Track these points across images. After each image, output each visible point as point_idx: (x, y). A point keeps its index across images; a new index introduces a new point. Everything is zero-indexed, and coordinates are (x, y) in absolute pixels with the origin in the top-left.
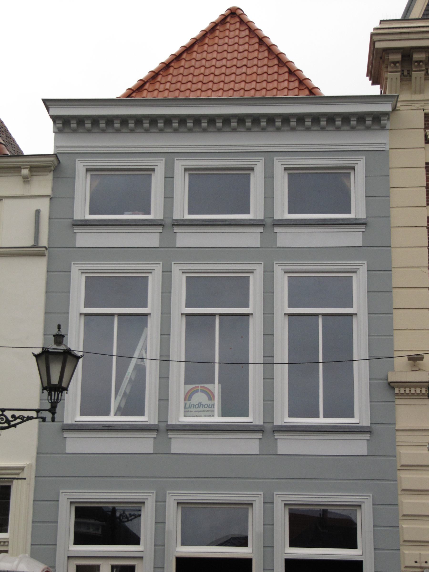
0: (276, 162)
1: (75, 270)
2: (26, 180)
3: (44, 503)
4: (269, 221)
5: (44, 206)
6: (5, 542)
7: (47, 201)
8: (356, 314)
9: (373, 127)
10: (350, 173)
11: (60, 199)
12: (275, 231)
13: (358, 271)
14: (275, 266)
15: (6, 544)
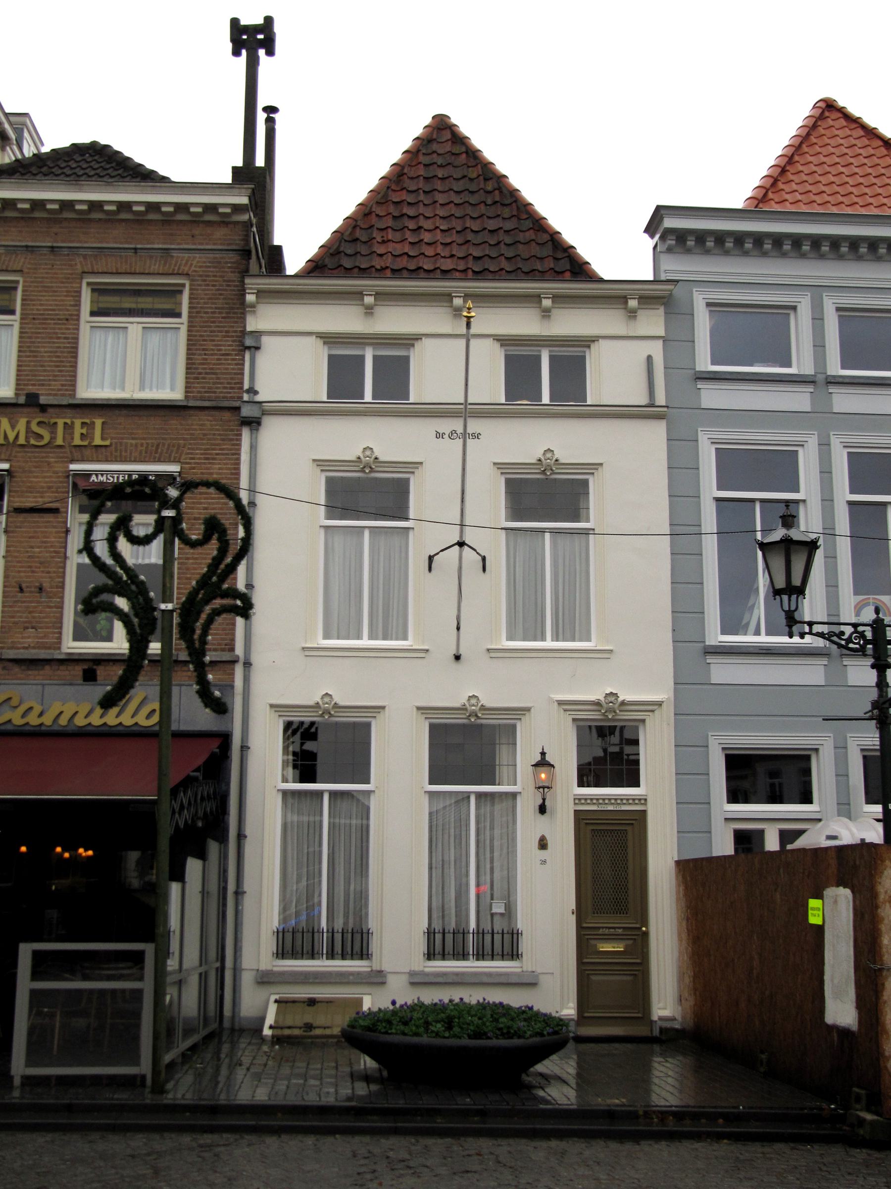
0: (695, 294)
1: (704, 439)
2: (632, 314)
3: (688, 747)
4: (820, 378)
5: (656, 350)
6: (640, 800)
7: (659, 344)
8: (804, 501)
9: (791, 255)
10: (789, 314)
11: (677, 341)
12: (830, 391)
13: (806, 444)
14: (832, 438)
15: (643, 802)
